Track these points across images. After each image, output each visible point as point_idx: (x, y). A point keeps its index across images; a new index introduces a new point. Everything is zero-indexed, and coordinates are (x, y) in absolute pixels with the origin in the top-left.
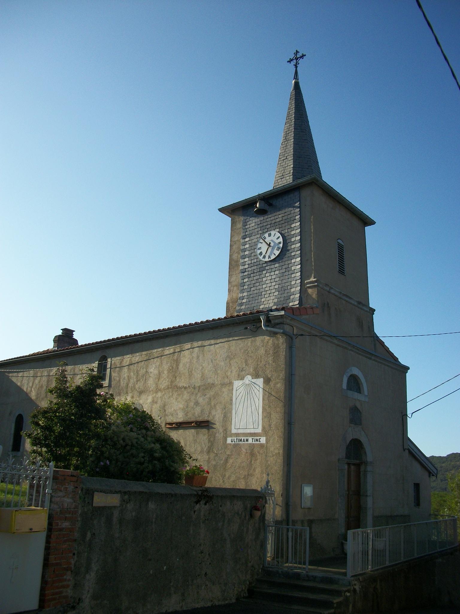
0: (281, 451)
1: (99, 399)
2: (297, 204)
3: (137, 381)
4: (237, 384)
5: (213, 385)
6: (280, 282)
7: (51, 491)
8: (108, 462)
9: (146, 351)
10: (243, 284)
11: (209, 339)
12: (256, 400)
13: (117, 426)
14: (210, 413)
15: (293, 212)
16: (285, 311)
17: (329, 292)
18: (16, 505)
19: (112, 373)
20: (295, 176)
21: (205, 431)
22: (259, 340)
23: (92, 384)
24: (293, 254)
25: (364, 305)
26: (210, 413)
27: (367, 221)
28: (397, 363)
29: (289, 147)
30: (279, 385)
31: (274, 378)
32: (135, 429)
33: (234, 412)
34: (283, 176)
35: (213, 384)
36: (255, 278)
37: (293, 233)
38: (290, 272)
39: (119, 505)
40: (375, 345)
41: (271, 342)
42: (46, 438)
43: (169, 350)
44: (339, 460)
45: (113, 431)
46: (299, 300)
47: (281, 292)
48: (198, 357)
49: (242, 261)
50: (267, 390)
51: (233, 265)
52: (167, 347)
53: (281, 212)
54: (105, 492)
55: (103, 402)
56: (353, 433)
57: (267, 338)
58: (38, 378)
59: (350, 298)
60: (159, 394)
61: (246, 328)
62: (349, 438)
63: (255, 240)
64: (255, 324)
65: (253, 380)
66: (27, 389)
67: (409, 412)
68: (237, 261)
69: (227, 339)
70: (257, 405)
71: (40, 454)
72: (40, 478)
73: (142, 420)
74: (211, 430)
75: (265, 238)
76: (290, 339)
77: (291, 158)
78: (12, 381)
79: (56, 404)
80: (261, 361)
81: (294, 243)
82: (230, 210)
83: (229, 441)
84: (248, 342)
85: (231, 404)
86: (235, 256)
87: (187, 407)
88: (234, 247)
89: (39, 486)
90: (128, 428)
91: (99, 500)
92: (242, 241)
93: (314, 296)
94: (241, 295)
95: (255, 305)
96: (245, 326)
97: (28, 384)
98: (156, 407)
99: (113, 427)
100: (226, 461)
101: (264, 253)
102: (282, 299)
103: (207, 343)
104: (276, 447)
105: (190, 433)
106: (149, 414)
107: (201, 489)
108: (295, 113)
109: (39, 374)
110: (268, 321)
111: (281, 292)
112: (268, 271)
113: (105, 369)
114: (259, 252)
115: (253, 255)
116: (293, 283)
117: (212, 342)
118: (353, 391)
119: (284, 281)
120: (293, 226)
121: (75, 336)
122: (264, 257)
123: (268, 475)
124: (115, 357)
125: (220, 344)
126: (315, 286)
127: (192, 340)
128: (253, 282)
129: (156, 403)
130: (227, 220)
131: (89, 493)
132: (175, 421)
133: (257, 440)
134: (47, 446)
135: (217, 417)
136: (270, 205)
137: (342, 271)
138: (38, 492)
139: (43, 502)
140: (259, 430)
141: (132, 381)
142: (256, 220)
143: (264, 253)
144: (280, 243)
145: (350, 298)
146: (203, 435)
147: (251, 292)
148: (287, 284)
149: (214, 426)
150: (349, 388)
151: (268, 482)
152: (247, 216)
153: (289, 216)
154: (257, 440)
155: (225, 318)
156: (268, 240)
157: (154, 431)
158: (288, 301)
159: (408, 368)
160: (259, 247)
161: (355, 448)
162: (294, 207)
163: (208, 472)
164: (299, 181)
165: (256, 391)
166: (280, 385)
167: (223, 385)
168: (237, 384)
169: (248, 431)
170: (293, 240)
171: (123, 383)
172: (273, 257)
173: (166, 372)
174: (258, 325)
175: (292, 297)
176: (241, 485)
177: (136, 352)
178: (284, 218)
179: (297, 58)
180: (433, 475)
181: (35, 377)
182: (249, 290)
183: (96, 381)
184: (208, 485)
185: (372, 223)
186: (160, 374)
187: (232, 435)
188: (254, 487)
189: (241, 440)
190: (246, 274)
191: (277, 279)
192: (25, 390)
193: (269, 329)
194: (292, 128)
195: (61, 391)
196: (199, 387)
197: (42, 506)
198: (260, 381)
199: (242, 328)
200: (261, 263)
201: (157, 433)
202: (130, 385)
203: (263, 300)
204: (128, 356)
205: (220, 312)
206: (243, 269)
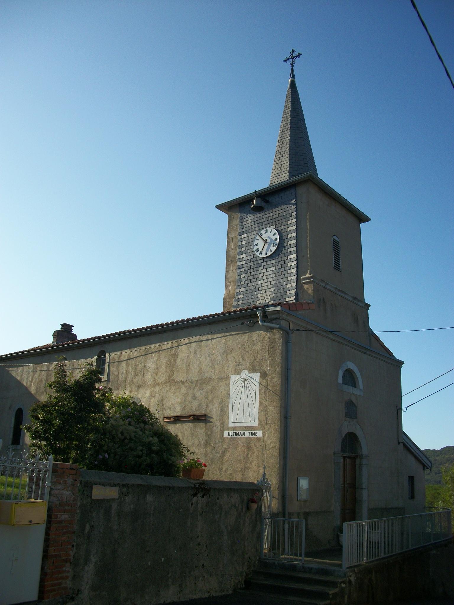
0: (277, 445)
1: (97, 394)
2: (293, 201)
3: (136, 376)
4: (234, 378)
5: (210, 379)
6: (276, 278)
7: (50, 484)
8: (106, 456)
9: (144, 345)
10: (240, 280)
11: (206, 334)
12: (253, 394)
13: (116, 420)
14: (207, 407)
15: (289, 209)
16: (281, 306)
17: (324, 288)
18: (16, 498)
19: (111, 367)
20: (291, 174)
21: (202, 424)
22: (256, 335)
23: (91, 378)
24: (289, 250)
25: (359, 301)
26: (207, 407)
27: (362, 218)
28: (391, 357)
29: (285, 144)
30: (275, 380)
31: (270, 372)
32: (133, 423)
33: (231, 406)
34: (279, 174)
35: (210, 379)
36: (252, 274)
37: (289, 229)
38: (286, 268)
39: (117, 498)
40: (370, 340)
41: (267, 337)
42: (45, 432)
43: (166, 345)
44: (334, 453)
45: (112, 424)
46: (295, 295)
47: (277, 288)
48: (195, 352)
49: (239, 257)
50: (264, 384)
51: (230, 261)
52: (165, 342)
53: (277, 209)
54: (103, 485)
55: (102, 396)
56: (348, 426)
57: (263, 333)
58: (38, 373)
59: (345, 294)
60: (157, 389)
61: (243, 323)
62: (345, 432)
63: (252, 237)
64: (252, 319)
65: (250, 375)
66: (27, 383)
67: (404, 406)
68: (234, 257)
69: (224, 334)
70: (254, 399)
71: (40, 447)
72: (39, 471)
73: (140, 414)
74: (208, 424)
75: (262, 235)
76: (287, 334)
77: (287, 156)
78: (12, 376)
79: (55, 398)
80: (258, 356)
81: (290, 239)
82: (227, 207)
83: (226, 434)
84: (245, 337)
85: (228, 398)
86: (232, 253)
87: (185, 401)
88: (231, 243)
89: (38, 479)
90: (127, 422)
91: (98, 492)
92: (239, 237)
93: (310, 292)
94: (238, 291)
95: (252, 300)
96: (241, 322)
97: (27, 379)
98: (154, 401)
99: (112, 421)
100: (223, 454)
101: (260, 250)
102: (279, 295)
103: (204, 338)
104: (273, 440)
105: (188, 427)
106: (147, 408)
107: (199, 482)
108: (291, 111)
109: (38, 369)
110: (265, 316)
111: (277, 288)
112: (265, 267)
113: (104, 363)
114: (255, 248)
115: (249, 251)
116: (289, 279)
117: (210, 337)
118: (349, 385)
119: (281, 277)
120: (289, 222)
121: (74, 331)
122: (261, 253)
123: (265, 468)
124: (114, 351)
125: (217, 339)
126: (311, 282)
127: (189, 335)
128: (250, 278)
129: (154, 397)
130: (224, 217)
131: (88, 486)
132: (172, 415)
133: (254, 434)
134: (46, 439)
135: (214, 411)
136: (267, 202)
137: (337, 267)
138: (37, 485)
139: (43, 494)
140: (256, 424)
141: (130, 375)
142: (253, 217)
143: (260, 250)
144: (276, 239)
145: (345, 294)
146: (200, 429)
147: (248, 288)
148: (283, 280)
149: (211, 420)
150: (345, 382)
151: (264, 475)
152: (244, 213)
153: (286, 213)
154: (254, 434)
155: (222, 313)
156: (264, 236)
157: (152, 425)
158: (284, 297)
159: (403, 363)
160: (255, 243)
161: (351, 442)
162: (290, 204)
163: (205, 465)
164: (296, 178)
165: (252, 385)
166: (276, 380)
167: (220, 379)
168: (234, 378)
169: (245, 425)
170: (289, 236)
171: (121, 378)
172: (269, 253)
173: (163, 367)
174: (255, 320)
175: (288, 293)
176: (238, 478)
177: (134, 347)
178: (280, 215)
179: (293, 57)
180: (427, 468)
181: (34, 371)
182: (245, 285)
183: (94, 375)
184: (205, 478)
185: (367, 219)
186: (157, 368)
187: (229, 429)
188: (250, 480)
189: (238, 434)
190: (242, 270)
191: (274, 275)
192: (25, 384)
193: (265, 324)
194: (288, 126)
195: (60, 385)
196: (197, 381)
197: (42, 499)
198: (257, 376)
199: (239, 323)
200: (258, 259)
201: (155, 427)
202: (128, 379)
203: (259, 296)
204: (126, 351)
205: (217, 308)
206: (240, 265)
